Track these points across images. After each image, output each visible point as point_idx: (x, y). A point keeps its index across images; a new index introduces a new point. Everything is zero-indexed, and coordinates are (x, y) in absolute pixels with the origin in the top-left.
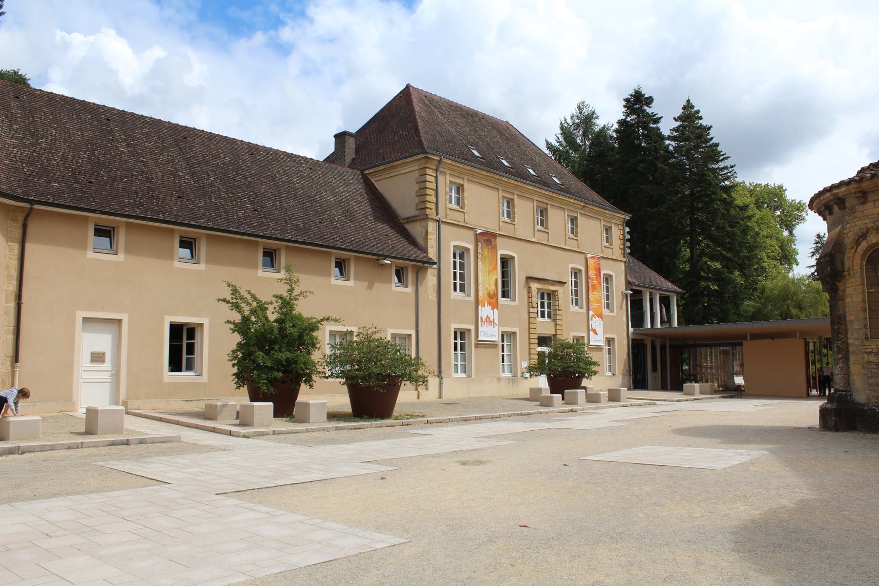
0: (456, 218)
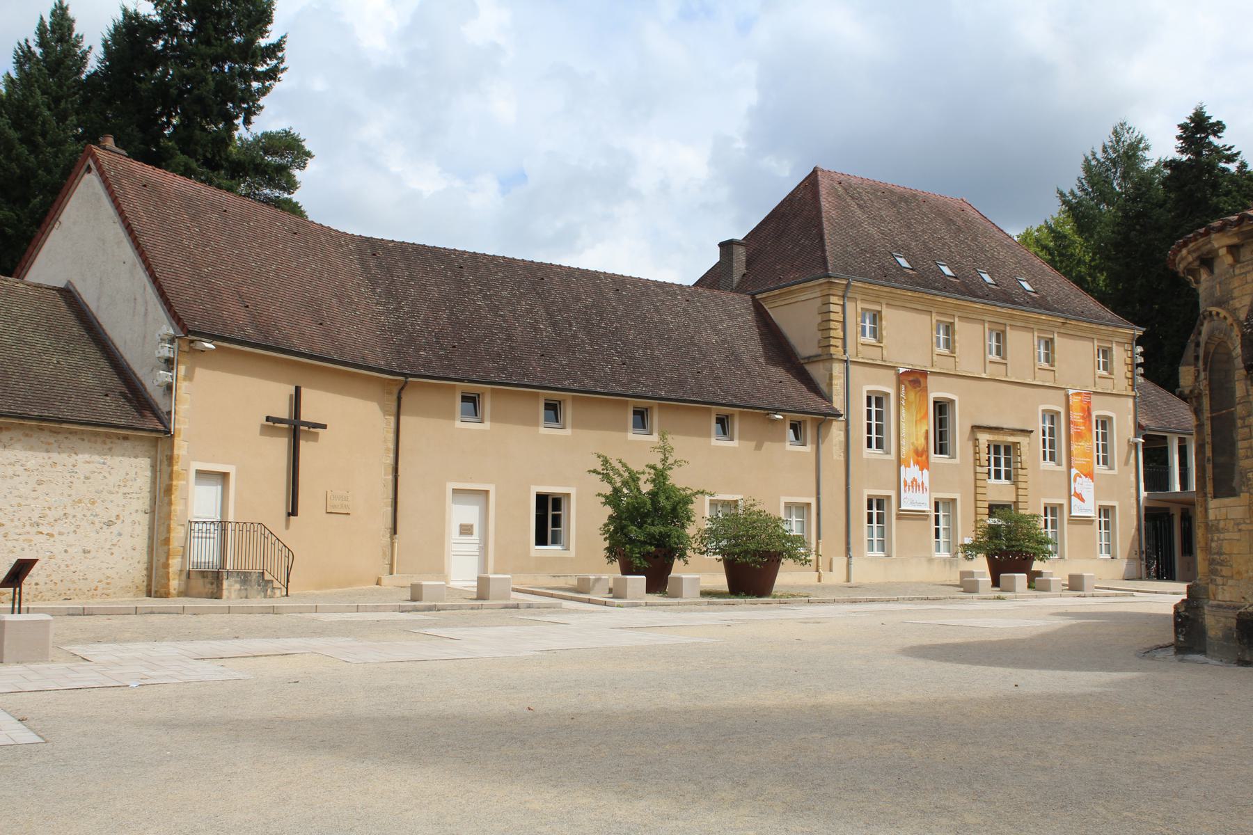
0: (873, 355)
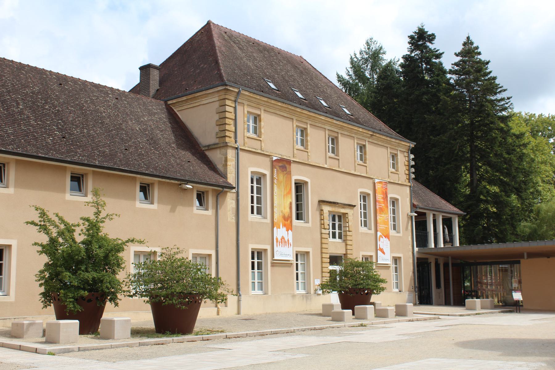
0: (253, 145)
